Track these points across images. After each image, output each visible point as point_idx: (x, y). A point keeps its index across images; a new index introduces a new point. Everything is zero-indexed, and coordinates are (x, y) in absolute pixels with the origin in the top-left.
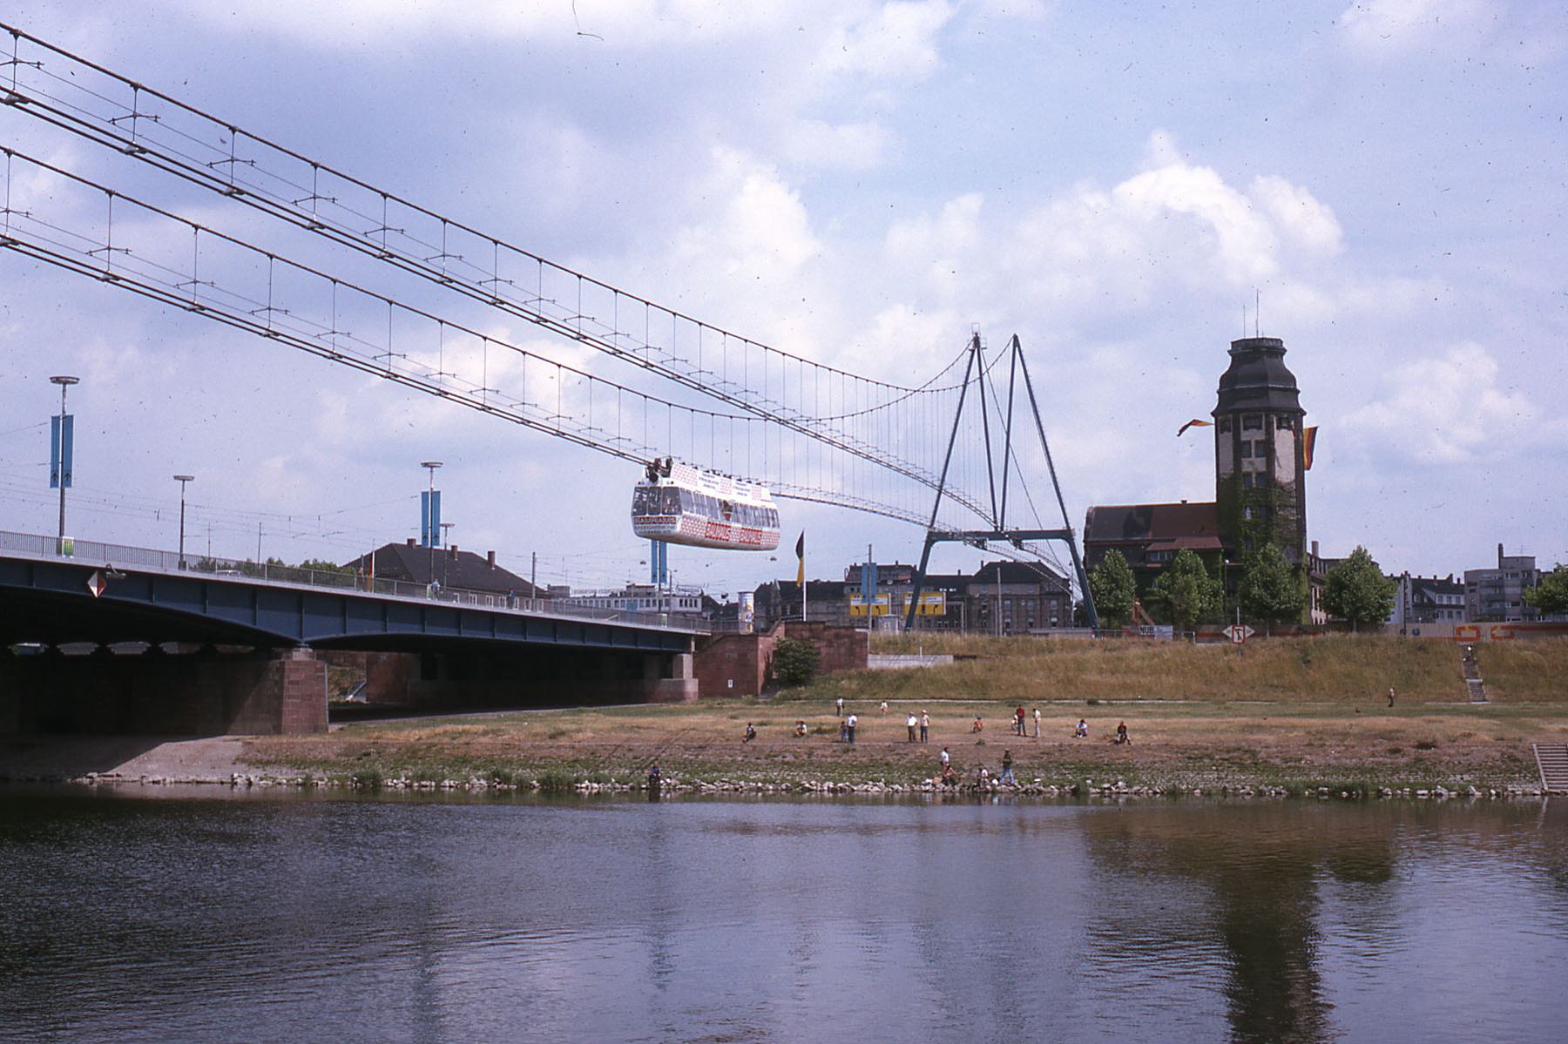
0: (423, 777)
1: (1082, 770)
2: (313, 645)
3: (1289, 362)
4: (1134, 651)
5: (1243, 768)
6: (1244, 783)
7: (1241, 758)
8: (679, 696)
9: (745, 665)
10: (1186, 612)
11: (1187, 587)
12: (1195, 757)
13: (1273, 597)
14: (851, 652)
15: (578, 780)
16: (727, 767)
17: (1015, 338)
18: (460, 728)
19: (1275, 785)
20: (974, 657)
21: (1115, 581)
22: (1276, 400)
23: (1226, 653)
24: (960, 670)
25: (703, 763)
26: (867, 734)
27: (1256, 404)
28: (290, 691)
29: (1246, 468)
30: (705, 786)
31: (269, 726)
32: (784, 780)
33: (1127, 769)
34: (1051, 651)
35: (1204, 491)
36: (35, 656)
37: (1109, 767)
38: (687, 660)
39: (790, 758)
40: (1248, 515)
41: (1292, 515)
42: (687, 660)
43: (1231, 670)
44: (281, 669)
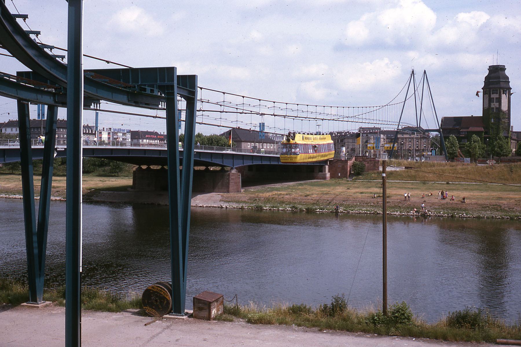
0: (273, 207)
1: (453, 210)
2: (236, 168)
3: (507, 72)
4: (459, 167)
5: (497, 211)
6: (498, 215)
7: (497, 208)
8: (324, 178)
9: (344, 169)
10: (475, 154)
11: (475, 148)
12: (484, 207)
13: (501, 151)
14: (374, 165)
15: (316, 209)
16: (356, 206)
17: (425, 71)
18: (279, 193)
19: (507, 216)
20: (411, 168)
21: (453, 144)
22: (502, 85)
23: (487, 168)
24: (407, 172)
25: (349, 205)
26: (392, 198)
27: (496, 86)
28: (231, 181)
29: (492, 106)
30: (351, 212)
31: (226, 190)
32: (372, 211)
33: (465, 210)
34: (434, 166)
35: (479, 113)
36: (144, 164)
37: (460, 209)
38: (327, 167)
39: (372, 204)
40: (492, 121)
41: (506, 121)
42: (327, 167)
43: (489, 173)
44: (229, 175)
